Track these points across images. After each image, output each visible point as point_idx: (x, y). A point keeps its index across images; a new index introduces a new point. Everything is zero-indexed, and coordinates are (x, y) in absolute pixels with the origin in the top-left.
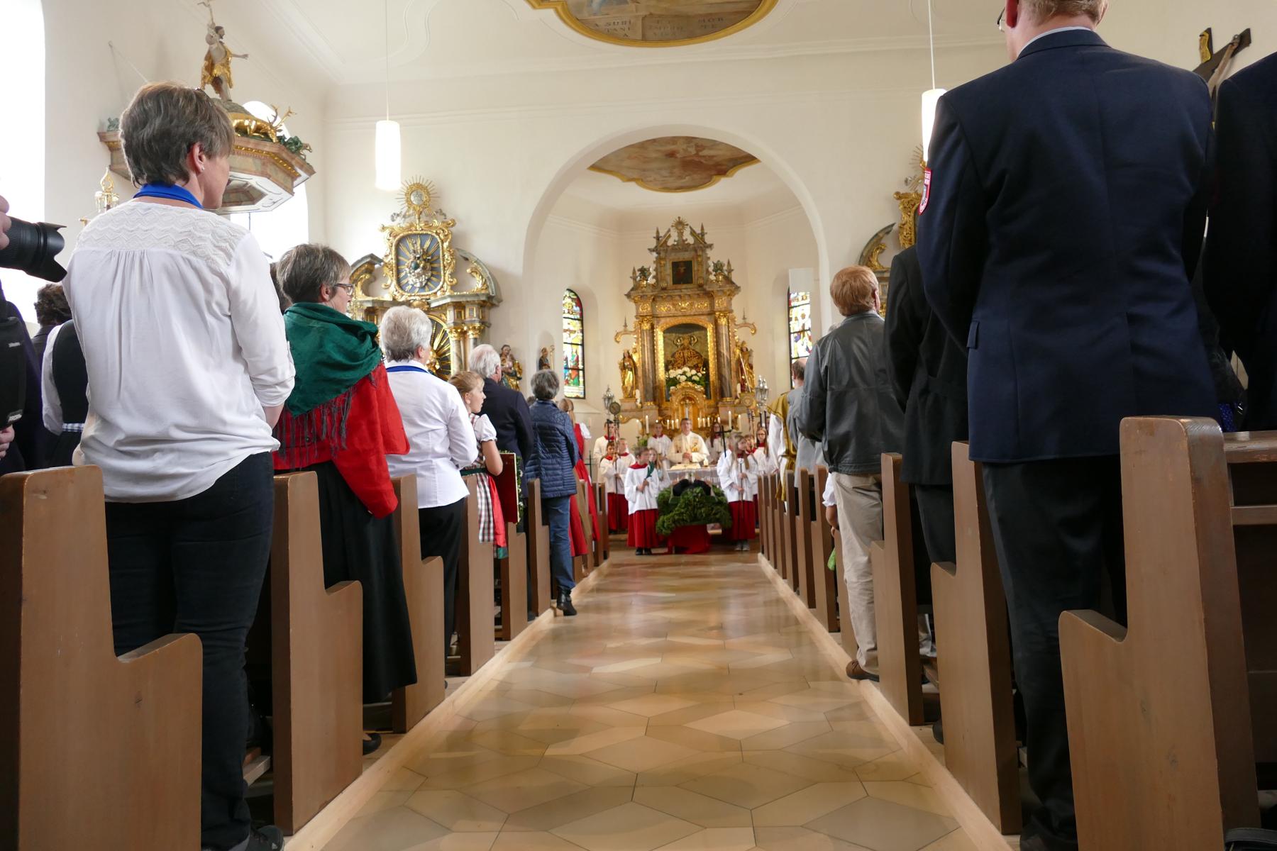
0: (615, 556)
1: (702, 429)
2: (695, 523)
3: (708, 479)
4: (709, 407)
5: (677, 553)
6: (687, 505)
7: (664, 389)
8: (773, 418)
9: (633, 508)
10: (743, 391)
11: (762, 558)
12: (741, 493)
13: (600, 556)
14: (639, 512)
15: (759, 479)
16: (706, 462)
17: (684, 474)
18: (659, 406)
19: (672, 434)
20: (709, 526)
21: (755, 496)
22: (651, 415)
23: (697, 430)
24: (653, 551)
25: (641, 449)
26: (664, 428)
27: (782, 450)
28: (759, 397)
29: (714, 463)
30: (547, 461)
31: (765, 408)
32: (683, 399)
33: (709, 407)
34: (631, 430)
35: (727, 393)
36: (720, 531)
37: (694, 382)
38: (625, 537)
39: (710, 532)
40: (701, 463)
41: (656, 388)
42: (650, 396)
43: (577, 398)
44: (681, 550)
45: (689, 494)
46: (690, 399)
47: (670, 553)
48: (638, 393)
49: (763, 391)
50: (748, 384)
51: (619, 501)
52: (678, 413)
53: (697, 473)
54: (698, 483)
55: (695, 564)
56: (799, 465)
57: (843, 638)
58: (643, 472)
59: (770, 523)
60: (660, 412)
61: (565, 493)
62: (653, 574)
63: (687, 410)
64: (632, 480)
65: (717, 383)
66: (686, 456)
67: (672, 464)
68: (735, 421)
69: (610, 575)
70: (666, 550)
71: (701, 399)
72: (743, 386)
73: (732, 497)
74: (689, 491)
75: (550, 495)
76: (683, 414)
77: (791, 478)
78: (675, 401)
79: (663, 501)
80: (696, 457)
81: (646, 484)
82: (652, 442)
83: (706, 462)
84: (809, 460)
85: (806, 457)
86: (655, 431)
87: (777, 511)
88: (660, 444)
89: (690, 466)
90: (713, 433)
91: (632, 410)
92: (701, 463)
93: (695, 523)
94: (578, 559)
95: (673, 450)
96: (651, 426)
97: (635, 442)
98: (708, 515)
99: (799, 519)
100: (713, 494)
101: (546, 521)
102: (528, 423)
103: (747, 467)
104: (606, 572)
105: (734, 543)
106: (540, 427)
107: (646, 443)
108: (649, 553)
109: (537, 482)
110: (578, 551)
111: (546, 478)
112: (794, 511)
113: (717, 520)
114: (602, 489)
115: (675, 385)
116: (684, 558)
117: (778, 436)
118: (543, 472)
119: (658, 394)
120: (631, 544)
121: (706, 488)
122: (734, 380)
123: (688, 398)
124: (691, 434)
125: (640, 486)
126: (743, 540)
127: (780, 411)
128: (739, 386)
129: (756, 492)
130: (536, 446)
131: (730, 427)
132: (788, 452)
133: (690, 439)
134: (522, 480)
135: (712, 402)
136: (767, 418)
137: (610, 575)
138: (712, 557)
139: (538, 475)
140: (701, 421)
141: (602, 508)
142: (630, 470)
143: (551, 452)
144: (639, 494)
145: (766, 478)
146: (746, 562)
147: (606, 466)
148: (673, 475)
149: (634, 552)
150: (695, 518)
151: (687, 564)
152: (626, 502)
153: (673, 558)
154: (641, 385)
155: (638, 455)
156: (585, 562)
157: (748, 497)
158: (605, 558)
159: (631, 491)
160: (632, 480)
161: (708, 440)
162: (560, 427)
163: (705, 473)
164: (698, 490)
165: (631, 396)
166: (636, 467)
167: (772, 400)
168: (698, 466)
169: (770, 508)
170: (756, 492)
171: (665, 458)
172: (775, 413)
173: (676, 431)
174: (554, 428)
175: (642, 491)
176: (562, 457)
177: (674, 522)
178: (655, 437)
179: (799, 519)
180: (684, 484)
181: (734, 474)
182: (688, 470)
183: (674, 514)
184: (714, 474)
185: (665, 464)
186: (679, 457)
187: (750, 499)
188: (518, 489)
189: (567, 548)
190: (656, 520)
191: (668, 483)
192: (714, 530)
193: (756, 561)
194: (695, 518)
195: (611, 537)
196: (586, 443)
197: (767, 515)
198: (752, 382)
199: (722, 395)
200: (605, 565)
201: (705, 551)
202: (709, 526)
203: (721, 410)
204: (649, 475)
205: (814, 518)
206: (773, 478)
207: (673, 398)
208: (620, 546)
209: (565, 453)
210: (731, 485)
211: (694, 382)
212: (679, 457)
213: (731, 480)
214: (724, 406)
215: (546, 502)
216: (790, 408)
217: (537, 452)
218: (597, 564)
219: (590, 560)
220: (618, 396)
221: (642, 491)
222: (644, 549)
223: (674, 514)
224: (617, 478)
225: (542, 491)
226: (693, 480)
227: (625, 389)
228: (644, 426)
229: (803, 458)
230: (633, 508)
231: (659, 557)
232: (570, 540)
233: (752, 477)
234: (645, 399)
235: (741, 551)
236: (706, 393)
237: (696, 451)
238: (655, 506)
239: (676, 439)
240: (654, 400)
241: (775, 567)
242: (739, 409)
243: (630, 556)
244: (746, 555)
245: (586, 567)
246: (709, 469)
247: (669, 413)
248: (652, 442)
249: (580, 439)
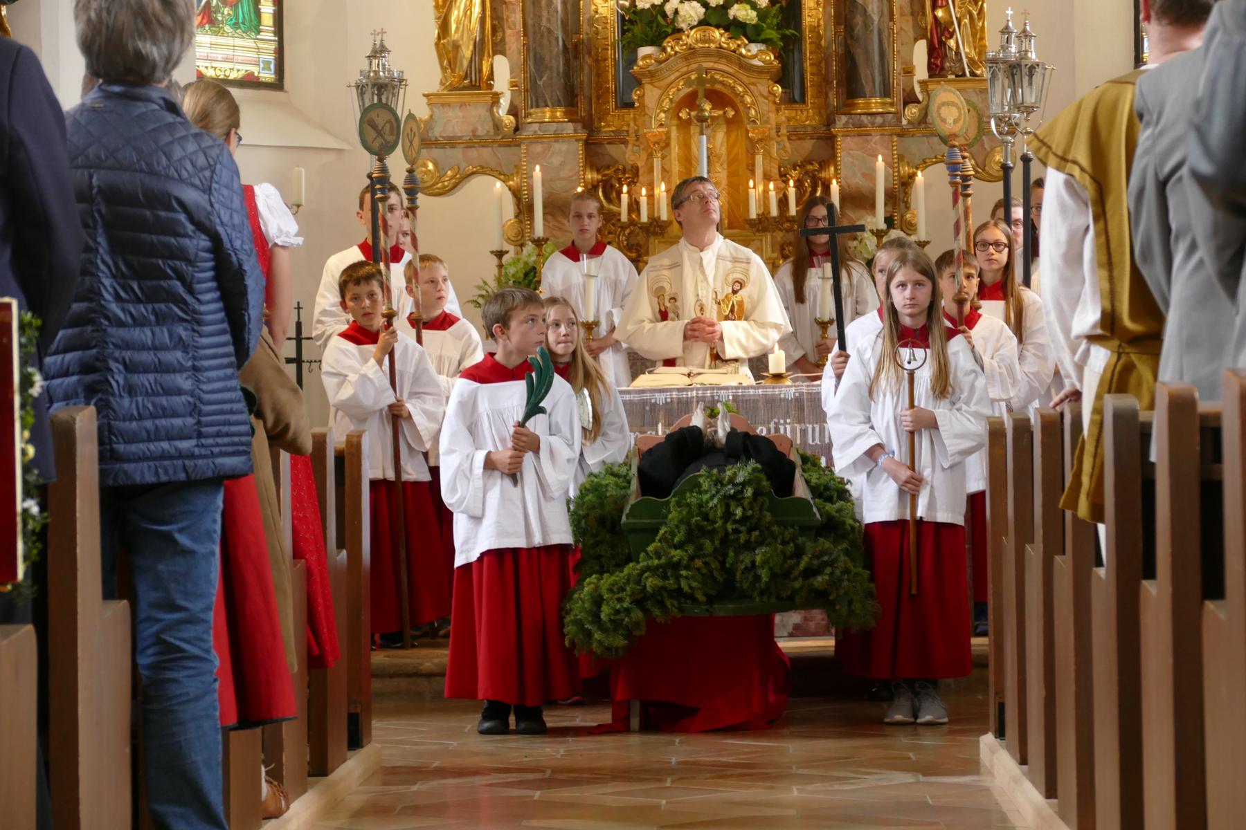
0: (394, 738)
1: (762, 224)
2: (723, 610)
3: (786, 430)
4: (796, 134)
5: (652, 725)
6: (695, 534)
7: (612, 55)
8: (1054, 180)
9: (471, 542)
10: (936, 69)
11: (996, 757)
12: (910, 488)
13: (334, 731)
14: (495, 557)
15: (996, 433)
16: (778, 361)
17: (685, 406)
18: (589, 125)
19: (640, 240)
20: (785, 620)
21: (975, 501)
22: (554, 164)
23: (742, 227)
24: (552, 719)
25: (513, 296)
26: (609, 217)
27: (1088, 317)
28: (1000, 99)
29: (808, 366)
30: (137, 334)
31: (1022, 145)
32: (690, 101)
33: (796, 134)
34: (469, 223)
35: (870, 75)
36: (827, 643)
37: (736, 28)
38: (437, 658)
39: (787, 645)
40: (758, 364)
41: (577, 50)
42: (551, 81)
43: (250, 82)
44: (663, 718)
45: (706, 487)
46: (719, 99)
47: (619, 727)
48: (502, 71)
49: (1017, 71)
50: (959, 43)
51: (416, 511)
52: (670, 149)
53: (741, 403)
54: (744, 445)
55: (721, 772)
56: (1173, 369)
57: (1059, 805)
58: (514, 394)
59: (1032, 609)
60: (593, 151)
61: (204, 467)
62: (548, 809)
63: (702, 145)
64: (473, 429)
65: (829, 34)
66: (697, 332)
67: (638, 364)
68: (899, 194)
69: (377, 810)
70: (604, 716)
71: (761, 101)
72: (937, 53)
73: (877, 504)
74: (703, 475)
75: (143, 473)
76: (688, 160)
77: (1132, 434)
78: (656, 102)
79: (597, 515)
80: (737, 338)
81: (525, 443)
82: (559, 274)
83: (778, 361)
84: (1217, 351)
85: (1206, 341)
86: (570, 232)
87: (1064, 564)
88: (591, 286)
89: (713, 377)
90: (809, 242)
91: (474, 142)
92: (758, 364)
93: (723, 610)
94: (247, 742)
95: (646, 309)
96: (555, 207)
97: (488, 271)
98: (781, 575)
99: (1156, 594)
100: (801, 490)
101: (118, 582)
102: (57, 180)
103: (943, 385)
104: (357, 800)
105: (886, 693)
106: (111, 195)
107: (531, 277)
108: (540, 730)
109: (85, 420)
110: (252, 707)
111: (125, 403)
112: (1137, 561)
113: (819, 598)
114: (348, 459)
115: (656, 40)
116: (678, 749)
117: (1072, 258)
118: (118, 379)
119: (585, 77)
120: (459, 689)
121: (776, 464)
122: (904, 25)
123: (710, 99)
124: (720, 245)
125: (504, 453)
126: (922, 681)
127: (1081, 154)
128: (920, 52)
129: (977, 481)
130: (88, 270)
131: (877, 220)
132: (1108, 329)
133: (714, 264)
134: (35, 406)
135: (808, 116)
136: (1034, 187)
137: (377, 810)
138: (792, 749)
139: (95, 391)
140: (761, 194)
141: (347, 538)
142: (462, 386)
143: (151, 297)
144: (499, 488)
145: (1022, 428)
146: (928, 769)
147: (346, 371)
148: (642, 411)
149: (472, 722)
150: (726, 589)
151: (689, 772)
152: (445, 517)
153: (633, 748)
154: (514, 41)
155: (496, 324)
156: (272, 754)
157: (941, 506)
158: (356, 741)
159: (464, 473)
160: (473, 429)
161: (786, 269)
162: (191, 196)
163: (773, 404)
164: (743, 471)
165: (474, 82)
166: (489, 372)
167: (1056, 109)
168: (745, 376)
169: (1035, 552)
170: (977, 481)
171: (718, 401)
172: (1064, 161)
173: (656, 228)
174: (165, 201)
175: (514, 476)
176: (195, 321)
177: (641, 601)
178: (573, 253)
179: (1156, 594)
180: (687, 449)
181: (886, 411)
182: (704, 388)
183: (641, 569)
184: (810, 409)
185: (611, 366)
186: (668, 337)
187: (949, 512)
188: (22, 446)
189: (206, 690)
190: (565, 592)
191: (619, 446)
192: (801, 638)
193: (972, 765)
194: (726, 589)
195: (380, 658)
196: (283, 262)
197: (1024, 578)
198: (977, 36)
199: (852, 88)
200: (351, 770)
201: (766, 722)
202: (785, 620)
203: (846, 148)
204: (534, 408)
205: (1150, 573)
206: (1052, 426)
207: (650, 94)
208: (416, 697)
209: (210, 305)
210: (873, 453)
211: (736, 28)
212: (668, 337)
213: (886, 435)
214: (861, 132)
215: (119, 501)
216: (1144, 136)
217: (93, 294)
218: (320, 767)
219: (293, 735)
220: (420, 78)
221: (514, 476)
222: (515, 710)
223: (641, 569)
224: (396, 417)
225: (107, 455)
226: (722, 430)
227: (446, 51)
228: (524, 208)
229: (1189, 344)
230: (471, 542)
231: (577, 744)
232: (217, 661)
233: (961, 427)
234: (531, 92)
235: (912, 725)
236: (783, 78)
237: (737, 313)
238: (562, 534)
239: (658, 261)
240: (570, 98)
241: (1051, 791)
242: (918, 146)
243: (459, 737)
244: (930, 741)
245: (276, 776)
246: (789, 389)
247: (630, 155)
248: (559, 274)
249: (264, 248)
